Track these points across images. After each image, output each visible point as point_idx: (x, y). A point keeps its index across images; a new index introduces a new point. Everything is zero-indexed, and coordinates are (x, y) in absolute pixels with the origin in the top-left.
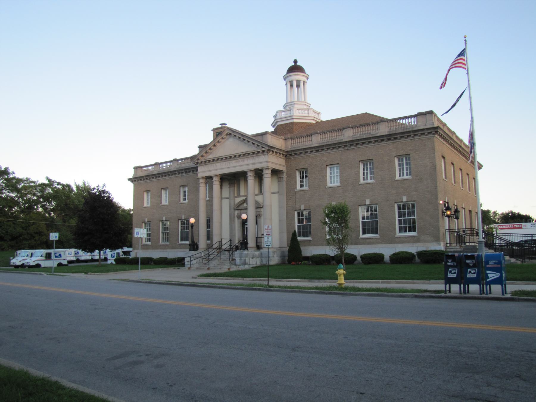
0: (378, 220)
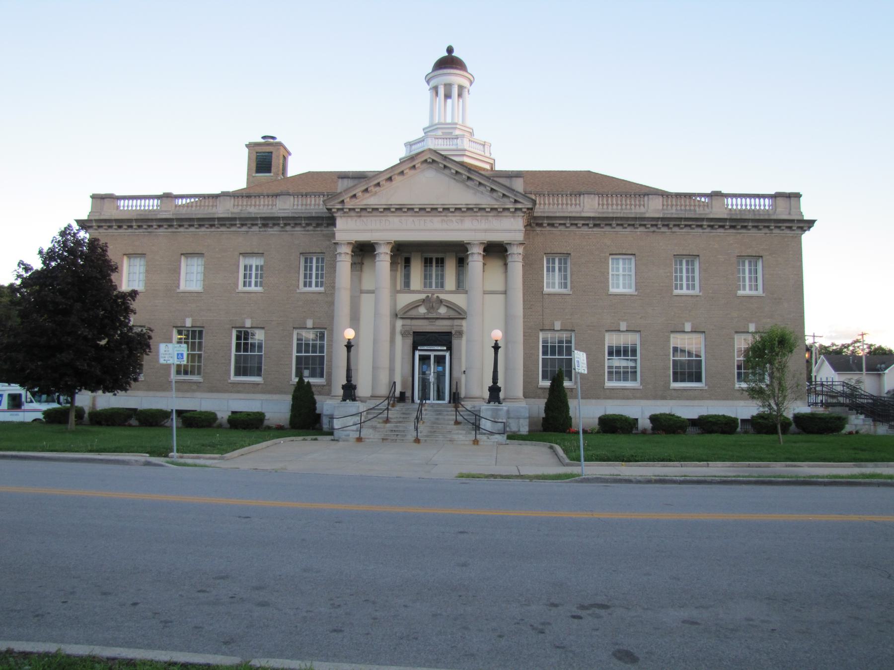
0: (263, 353)
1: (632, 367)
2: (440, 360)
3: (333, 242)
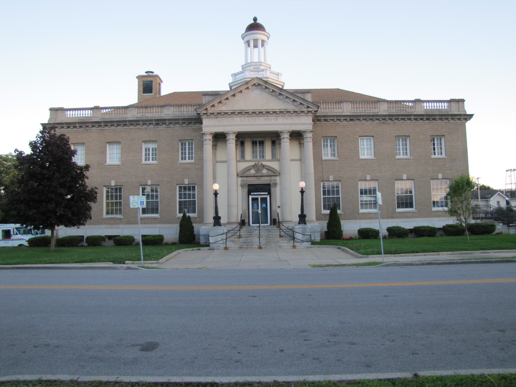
1: (374, 201)
2: (264, 200)
3: (202, 133)
